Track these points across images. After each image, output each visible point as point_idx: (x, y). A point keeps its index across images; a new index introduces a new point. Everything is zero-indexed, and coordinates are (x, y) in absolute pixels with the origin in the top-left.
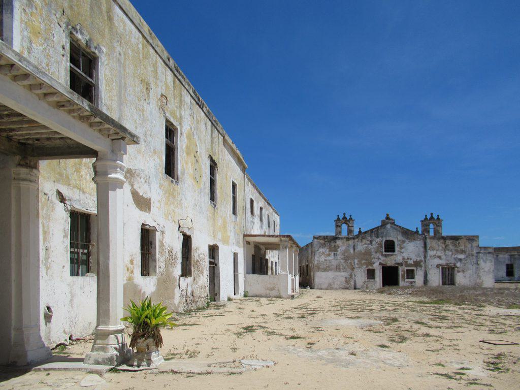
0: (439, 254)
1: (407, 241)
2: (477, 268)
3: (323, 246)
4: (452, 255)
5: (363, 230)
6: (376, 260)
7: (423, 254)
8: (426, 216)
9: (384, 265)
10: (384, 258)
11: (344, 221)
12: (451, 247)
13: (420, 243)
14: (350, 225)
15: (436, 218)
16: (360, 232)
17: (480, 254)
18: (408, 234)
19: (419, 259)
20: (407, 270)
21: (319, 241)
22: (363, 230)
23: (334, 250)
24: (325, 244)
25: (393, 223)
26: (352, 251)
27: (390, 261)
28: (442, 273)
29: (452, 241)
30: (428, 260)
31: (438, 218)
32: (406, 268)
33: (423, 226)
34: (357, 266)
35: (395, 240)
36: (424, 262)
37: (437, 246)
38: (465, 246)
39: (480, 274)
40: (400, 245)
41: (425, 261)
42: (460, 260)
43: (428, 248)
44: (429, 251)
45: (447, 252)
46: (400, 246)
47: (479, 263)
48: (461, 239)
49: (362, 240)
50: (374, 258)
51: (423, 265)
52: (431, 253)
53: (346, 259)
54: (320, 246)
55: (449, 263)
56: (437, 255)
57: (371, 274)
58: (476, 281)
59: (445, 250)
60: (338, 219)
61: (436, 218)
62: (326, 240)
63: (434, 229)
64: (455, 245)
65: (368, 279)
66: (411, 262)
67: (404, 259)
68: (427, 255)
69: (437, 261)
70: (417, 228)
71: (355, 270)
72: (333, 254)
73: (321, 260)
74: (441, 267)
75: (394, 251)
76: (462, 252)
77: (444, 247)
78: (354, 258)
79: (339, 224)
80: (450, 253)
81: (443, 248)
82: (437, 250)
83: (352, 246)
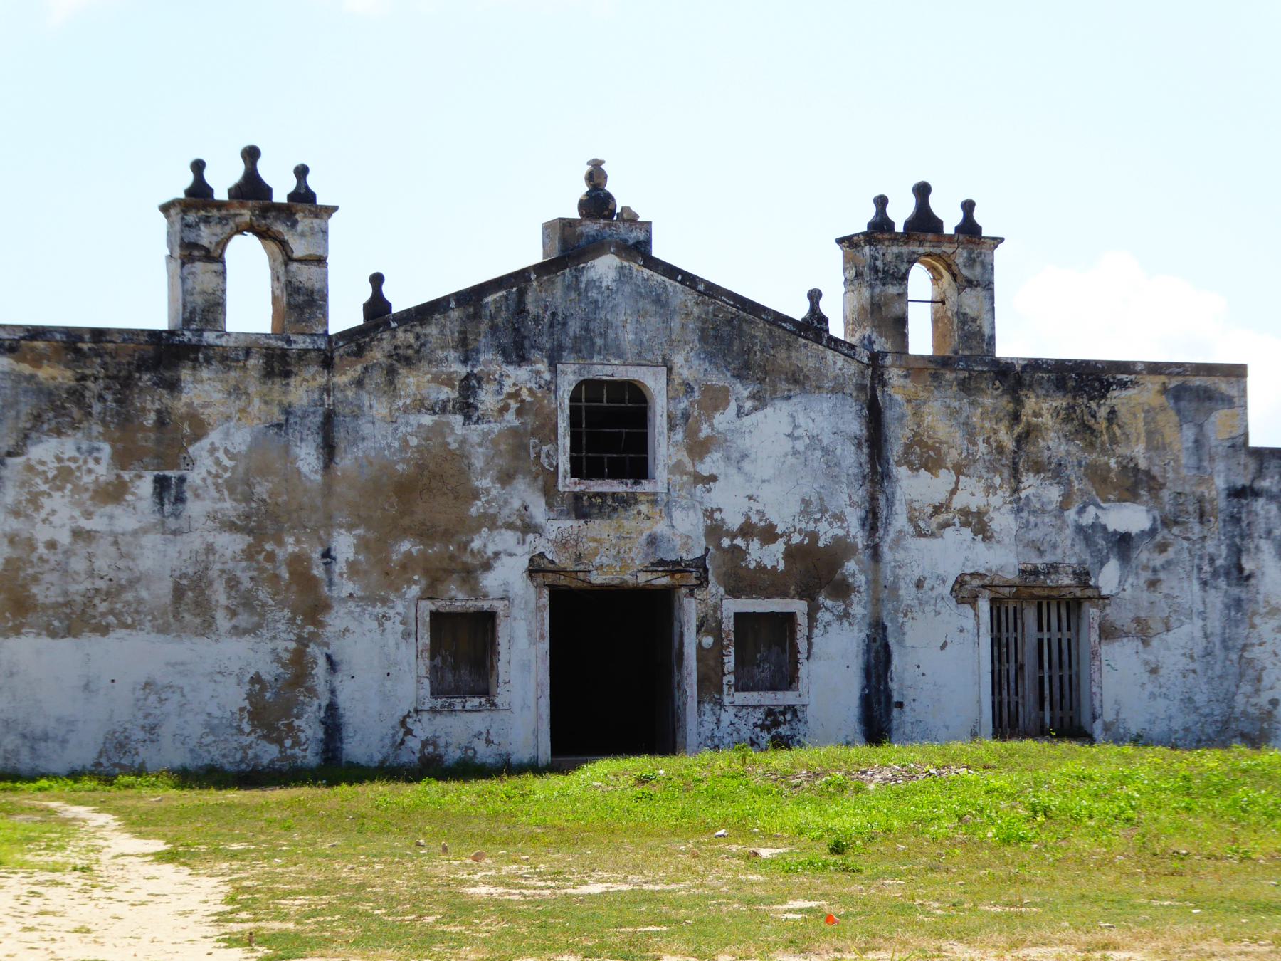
0: (971, 495)
1: (742, 391)
2: (1238, 604)
3: (59, 410)
4: (1064, 505)
5: (400, 299)
6: (507, 539)
7: (860, 494)
8: (881, 202)
9: (563, 581)
10: (569, 524)
11: (246, 215)
12: (1054, 444)
13: (831, 420)
14: (299, 248)
15: (951, 220)
16: (377, 307)
17: (1260, 504)
18: (744, 338)
19: (827, 533)
20: (738, 616)
21: (26, 369)
22: (400, 299)
23: (161, 450)
24: (77, 395)
25: (639, 250)
26: (307, 457)
27: (614, 552)
28: (996, 643)
29: (1061, 402)
30: (897, 543)
31: (969, 228)
32: (733, 606)
33: (855, 278)
34: (347, 587)
35: (654, 382)
36: (864, 556)
37: (958, 436)
38: (1155, 444)
39: (1255, 652)
40: (686, 416)
41: (875, 553)
42: (1123, 543)
43: (895, 450)
44: (901, 472)
45: (1031, 484)
46: (691, 433)
47: (1248, 565)
48: (1124, 385)
49: (391, 372)
50: (490, 521)
51: (860, 580)
52: (914, 487)
53: (259, 525)
54: (38, 418)
55: (1040, 562)
56: (958, 502)
57: (463, 648)
58: (1230, 700)
59: (1015, 474)
60: (199, 192)
61: (951, 220)
62: (94, 367)
63: (940, 302)
64: (1085, 431)
65: (435, 693)
66: (771, 556)
67: (715, 531)
68: (890, 502)
69: (953, 554)
70: (815, 296)
71: (336, 620)
72: (145, 486)
73: (42, 534)
74: (984, 606)
75: (639, 469)
76: (1135, 483)
77: (1010, 445)
78: (329, 523)
79: (206, 236)
80: (1054, 494)
81: (1000, 449)
82: (959, 470)
83: (318, 419)
